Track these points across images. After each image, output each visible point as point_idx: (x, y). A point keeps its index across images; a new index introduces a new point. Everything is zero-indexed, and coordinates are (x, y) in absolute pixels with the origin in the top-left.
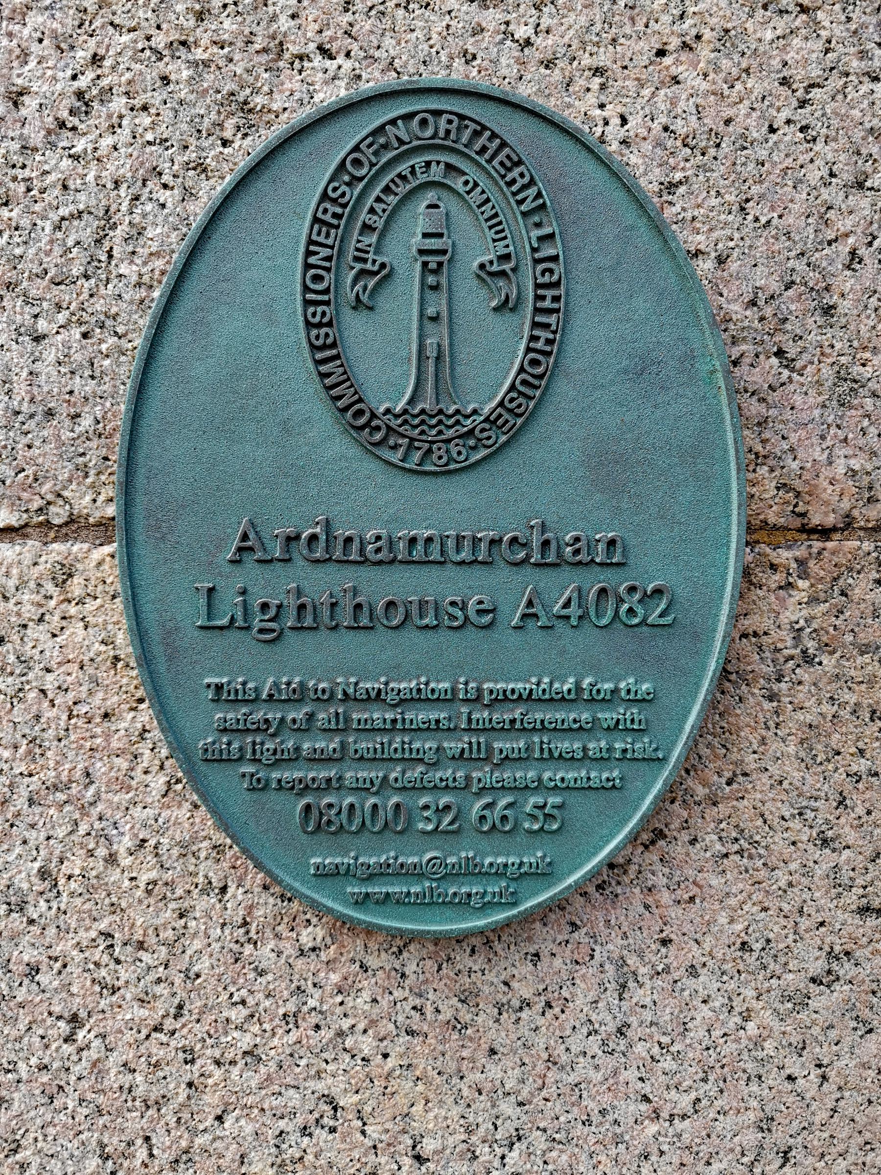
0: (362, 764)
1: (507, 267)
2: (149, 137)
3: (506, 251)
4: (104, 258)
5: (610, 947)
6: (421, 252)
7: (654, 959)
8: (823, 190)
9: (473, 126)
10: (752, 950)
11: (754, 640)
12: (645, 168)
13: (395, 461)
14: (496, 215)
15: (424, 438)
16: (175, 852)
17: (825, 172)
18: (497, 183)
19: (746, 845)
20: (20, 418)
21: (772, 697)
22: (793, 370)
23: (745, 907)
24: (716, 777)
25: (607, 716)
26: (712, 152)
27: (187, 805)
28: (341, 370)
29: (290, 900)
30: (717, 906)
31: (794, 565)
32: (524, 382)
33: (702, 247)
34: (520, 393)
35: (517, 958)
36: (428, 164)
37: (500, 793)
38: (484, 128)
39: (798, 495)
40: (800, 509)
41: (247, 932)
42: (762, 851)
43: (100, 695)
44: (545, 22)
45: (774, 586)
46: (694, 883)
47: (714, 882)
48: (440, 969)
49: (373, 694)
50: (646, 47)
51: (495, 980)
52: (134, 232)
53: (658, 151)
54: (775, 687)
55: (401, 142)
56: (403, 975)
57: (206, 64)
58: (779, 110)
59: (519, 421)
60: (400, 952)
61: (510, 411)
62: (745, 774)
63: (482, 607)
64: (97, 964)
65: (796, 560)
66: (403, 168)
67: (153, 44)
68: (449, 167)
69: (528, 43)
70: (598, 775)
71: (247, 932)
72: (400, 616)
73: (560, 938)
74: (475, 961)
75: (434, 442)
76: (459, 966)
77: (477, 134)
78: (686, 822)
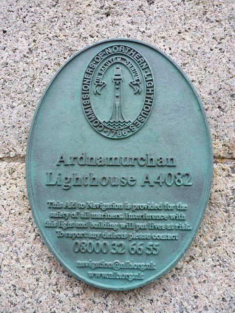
0: (93, 230)
1: (138, 83)
2: (46, 58)
3: (138, 79)
4: (32, 87)
5: (177, 298)
6: (114, 79)
7: (192, 303)
8: (227, 64)
9: (128, 49)
10: (226, 301)
11: (219, 193)
12: (178, 60)
13: (106, 136)
14: (135, 70)
15: (115, 130)
16: (36, 259)
17: (227, 60)
18: (135, 63)
19: (221, 263)
20: (6, 128)
21: (227, 211)
22: (224, 112)
23: (223, 285)
24: (210, 238)
25: (173, 215)
26: (195, 56)
27: (41, 243)
28: (91, 111)
29: (71, 277)
30: (213, 284)
31: (230, 169)
32: (144, 113)
33: (194, 79)
34: (143, 116)
35: (145, 301)
36: (116, 58)
37: (138, 240)
38: (132, 49)
39: (229, 148)
40: (230, 152)
41: (57, 287)
42: (227, 265)
43: (19, 207)
44: (148, 27)
45: (224, 175)
46: (205, 276)
47: (211, 276)
48: (119, 304)
49: (98, 206)
50: (175, 32)
51: (138, 309)
52: (40, 80)
53: (180, 56)
54: (228, 208)
55: (109, 53)
56: (107, 305)
57: (61, 40)
58: (213, 45)
59: (142, 124)
60: (106, 297)
61: (139, 121)
62: (220, 238)
63: (132, 179)
64: (10, 296)
65: (231, 167)
66: (110, 59)
67: (48, 37)
68: (122, 58)
69: (144, 32)
70: (170, 235)
71: (57, 287)
72: (107, 182)
73: (160, 294)
74: (131, 301)
75: (117, 130)
76: (126, 303)
77: (129, 50)
78: (201, 254)
